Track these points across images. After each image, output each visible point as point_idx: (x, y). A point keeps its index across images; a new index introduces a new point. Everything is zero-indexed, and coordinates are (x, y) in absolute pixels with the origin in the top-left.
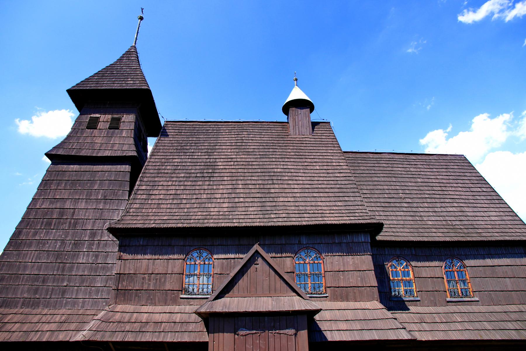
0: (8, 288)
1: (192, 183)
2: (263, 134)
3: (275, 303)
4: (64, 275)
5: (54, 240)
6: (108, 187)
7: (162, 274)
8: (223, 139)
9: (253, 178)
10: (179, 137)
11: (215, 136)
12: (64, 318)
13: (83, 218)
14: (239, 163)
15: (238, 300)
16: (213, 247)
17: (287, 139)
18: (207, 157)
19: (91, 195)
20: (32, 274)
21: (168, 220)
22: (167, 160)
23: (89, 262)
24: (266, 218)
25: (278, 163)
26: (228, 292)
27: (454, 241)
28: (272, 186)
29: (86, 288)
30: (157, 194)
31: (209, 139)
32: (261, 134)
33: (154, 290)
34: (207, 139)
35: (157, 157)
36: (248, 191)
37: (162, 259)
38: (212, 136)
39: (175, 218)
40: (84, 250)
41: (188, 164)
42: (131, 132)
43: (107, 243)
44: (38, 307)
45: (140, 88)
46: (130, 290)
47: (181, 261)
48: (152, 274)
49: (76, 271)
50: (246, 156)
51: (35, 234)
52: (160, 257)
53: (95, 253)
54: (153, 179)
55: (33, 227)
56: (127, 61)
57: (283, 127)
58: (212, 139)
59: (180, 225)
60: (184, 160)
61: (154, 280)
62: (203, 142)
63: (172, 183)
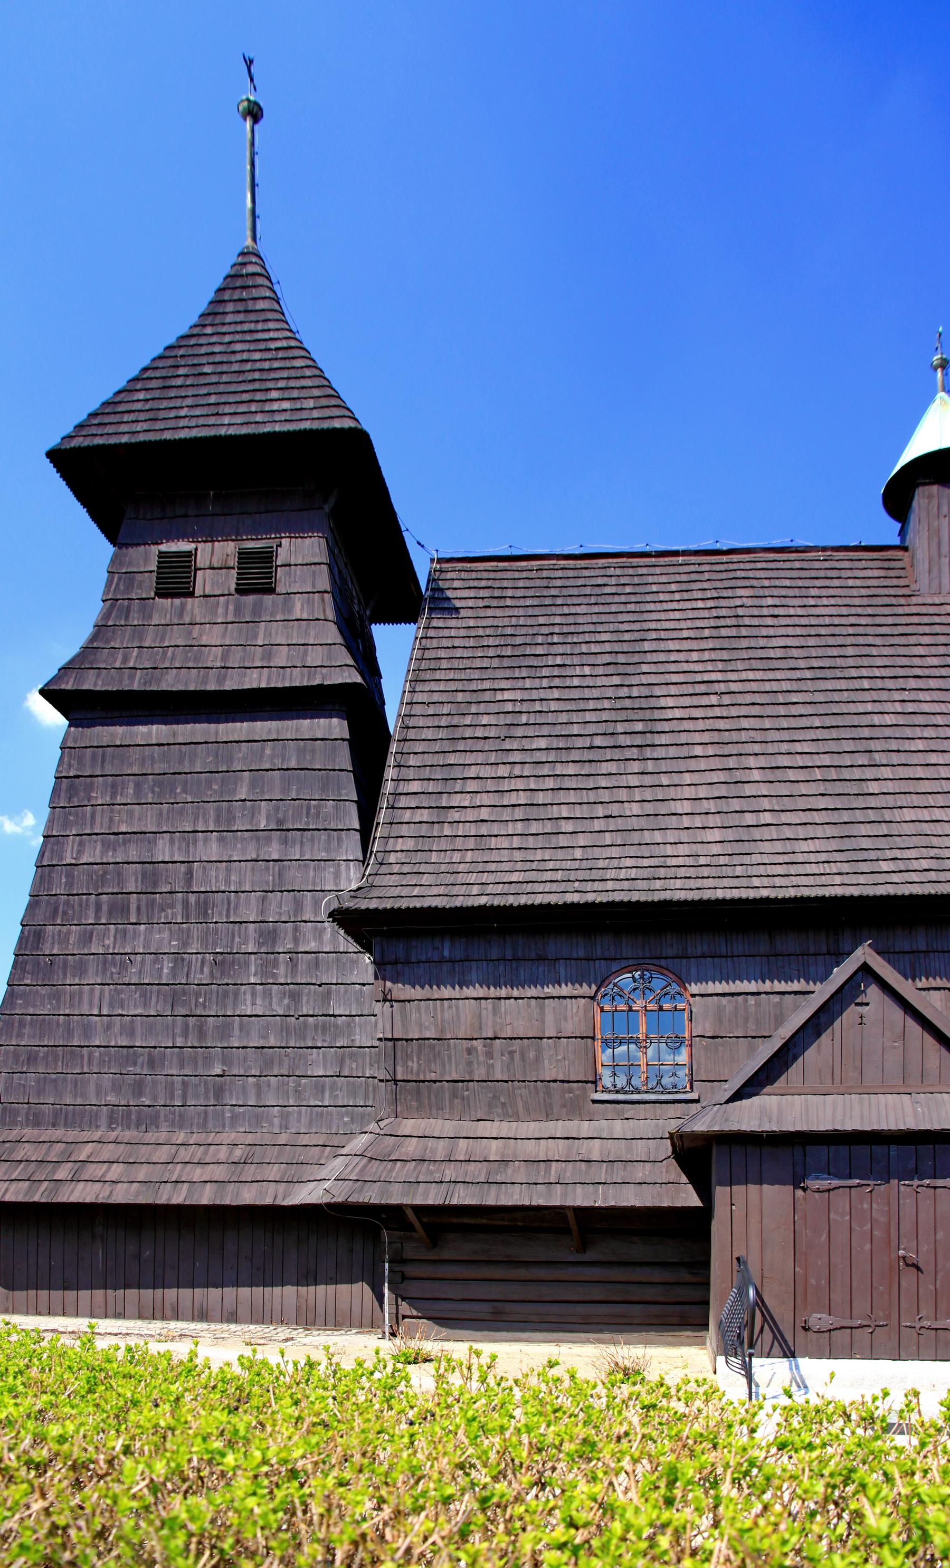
0: (55, 1081)
1: (581, 769)
2: (813, 592)
3: (926, 1110)
4: (207, 1048)
5: (150, 954)
6: (283, 791)
7: (528, 1038)
8: (662, 616)
9: (798, 747)
10: (499, 613)
11: (631, 607)
13: (223, 888)
14: (740, 699)
15: (806, 1101)
16: (684, 961)
17: (907, 610)
18: (616, 680)
19: (232, 819)
20: (113, 1047)
21: (527, 882)
22: (475, 695)
23: (274, 1013)
24: (862, 873)
25: (884, 695)
26: (771, 1080)
28: (869, 773)
29: (283, 1081)
30: (466, 807)
31: (611, 618)
32: (804, 592)
33: (507, 1082)
34: (604, 618)
35: (434, 686)
36: (784, 789)
37: (523, 998)
38: (622, 608)
39: (548, 876)
40: (252, 980)
41: (554, 706)
42: (323, 600)
43: (317, 958)
44: (157, 1127)
45: (326, 425)
46: (435, 1082)
47: (582, 1001)
48: (496, 1038)
49: (240, 1037)
50: (759, 675)
51: (87, 938)
52: (515, 993)
53: (287, 987)
54: (440, 760)
55: (73, 920)
56: (240, 317)
57: (886, 564)
58: (621, 618)
59: (575, 898)
60: (535, 695)
61: (502, 1055)
62: (591, 628)
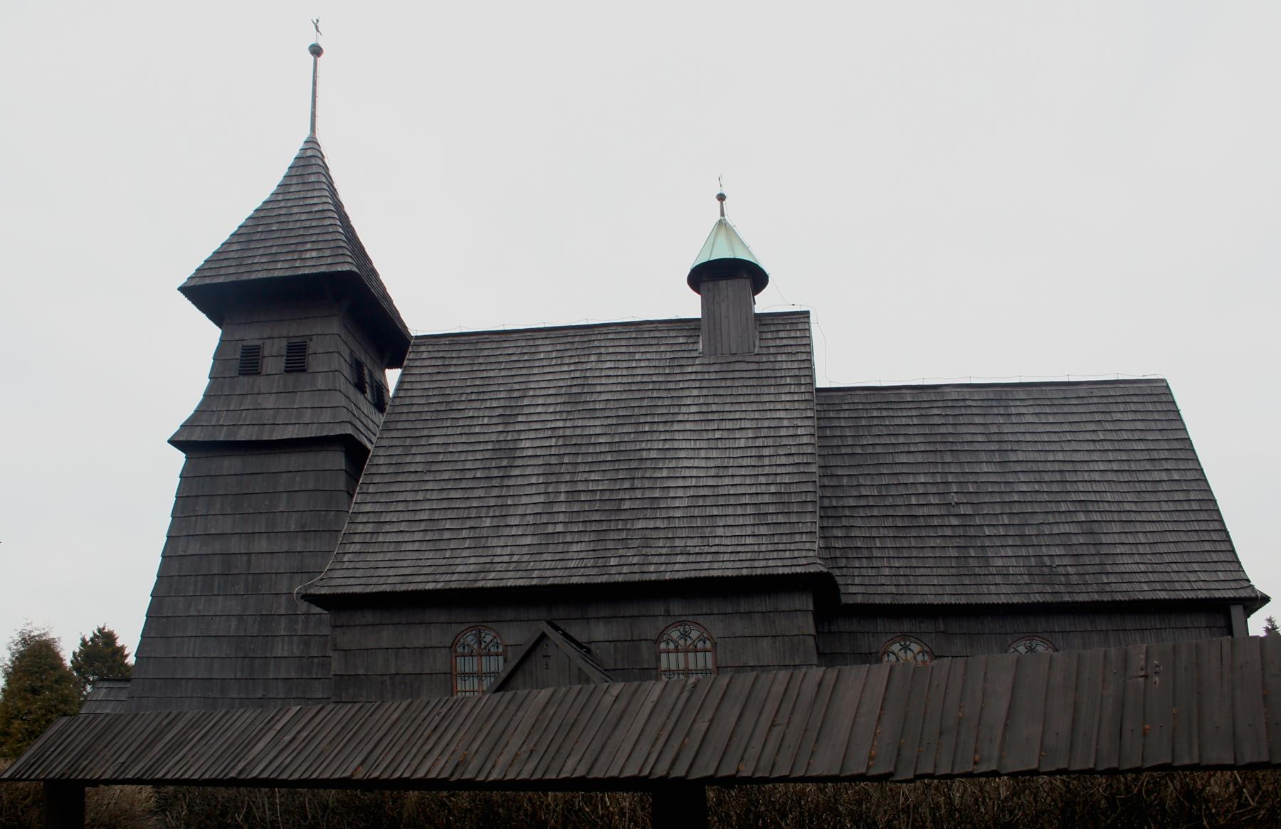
9: (593, 477)
18: (500, 428)
23: (294, 655)
27: (998, 604)
30: (394, 522)
35: (394, 434)
40: (282, 633)
48: (397, 674)
63: (426, 494)
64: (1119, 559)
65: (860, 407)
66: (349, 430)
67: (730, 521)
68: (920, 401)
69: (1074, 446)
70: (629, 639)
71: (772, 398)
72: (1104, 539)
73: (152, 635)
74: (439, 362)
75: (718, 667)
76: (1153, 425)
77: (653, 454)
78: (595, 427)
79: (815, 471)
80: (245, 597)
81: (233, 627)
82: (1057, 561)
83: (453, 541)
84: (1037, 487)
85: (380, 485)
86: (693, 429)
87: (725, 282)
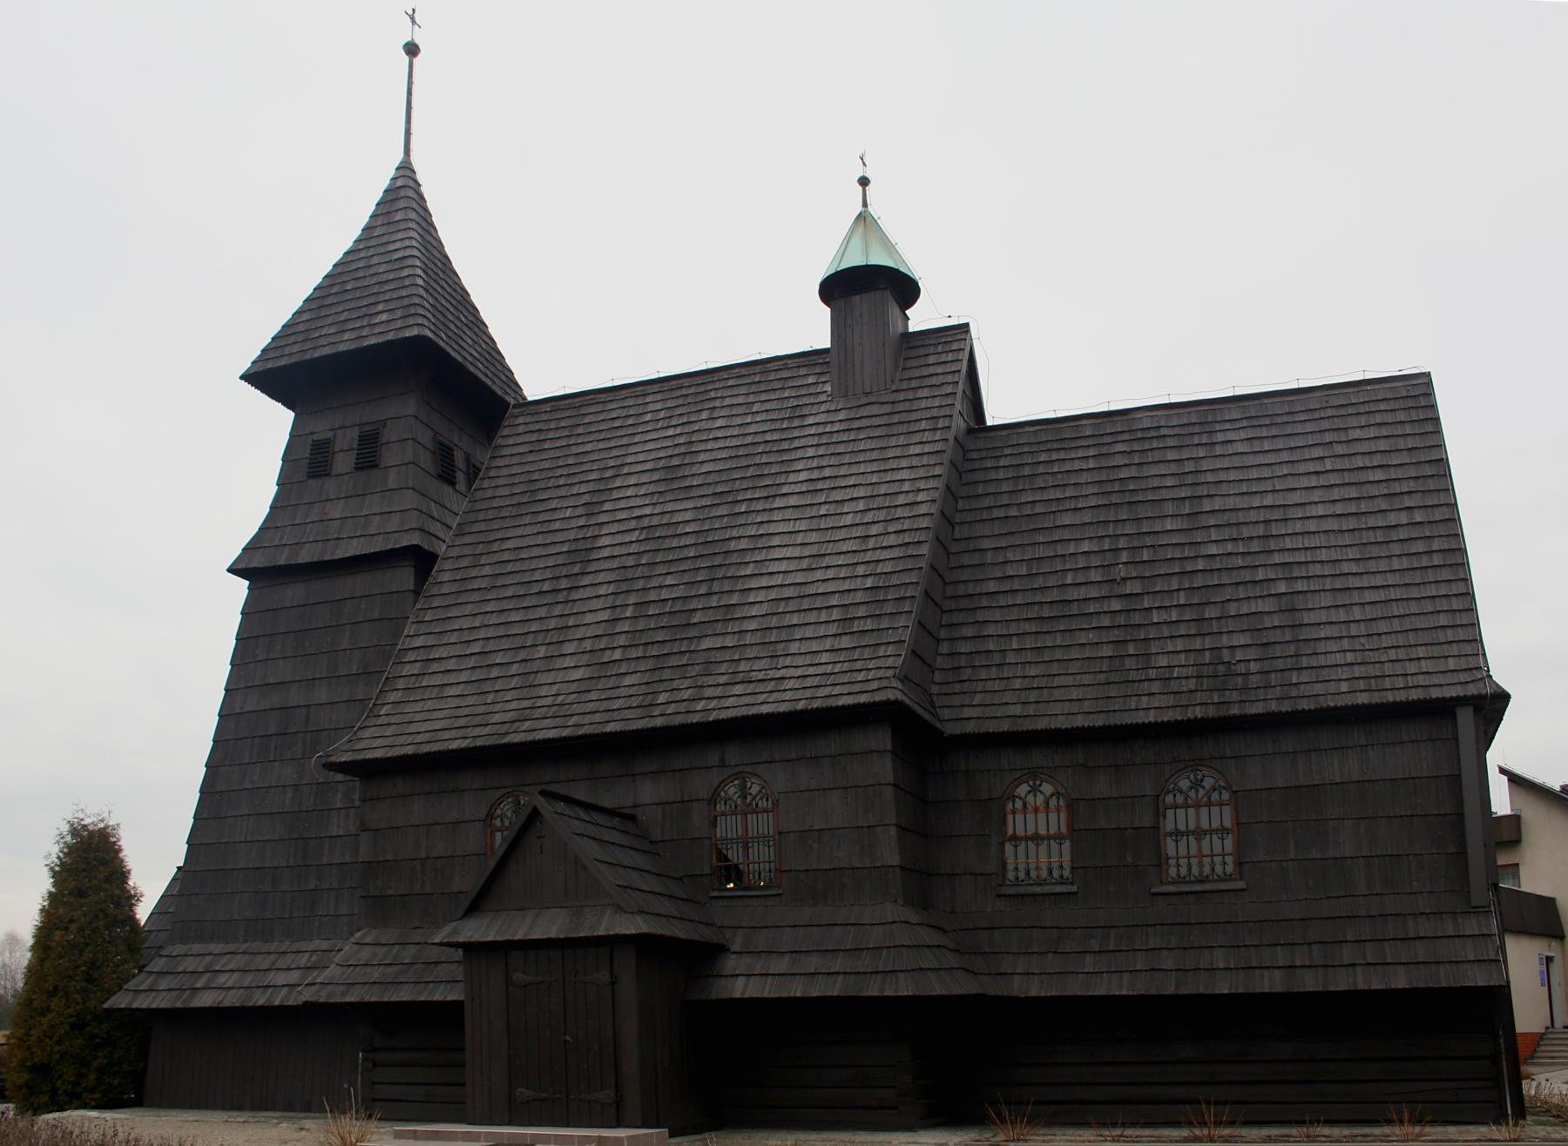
12: (314, 958)
18: (582, 522)
27: (1144, 723)
35: (467, 539)
40: (338, 806)
48: (428, 858)
64: (1322, 646)
65: (1025, 450)
66: (415, 539)
67: (809, 632)
68: (1102, 435)
69: (1290, 483)
70: (679, 799)
71: (898, 452)
72: (1307, 618)
73: (205, 816)
74: (534, 437)
75: (780, 833)
76: (1401, 444)
77: (743, 544)
78: (684, 511)
79: (925, 553)
80: (302, 761)
81: (288, 801)
82: (1239, 655)
83: (501, 680)
84: (1230, 547)
85: (439, 609)
86: (797, 504)
87: (858, 297)
